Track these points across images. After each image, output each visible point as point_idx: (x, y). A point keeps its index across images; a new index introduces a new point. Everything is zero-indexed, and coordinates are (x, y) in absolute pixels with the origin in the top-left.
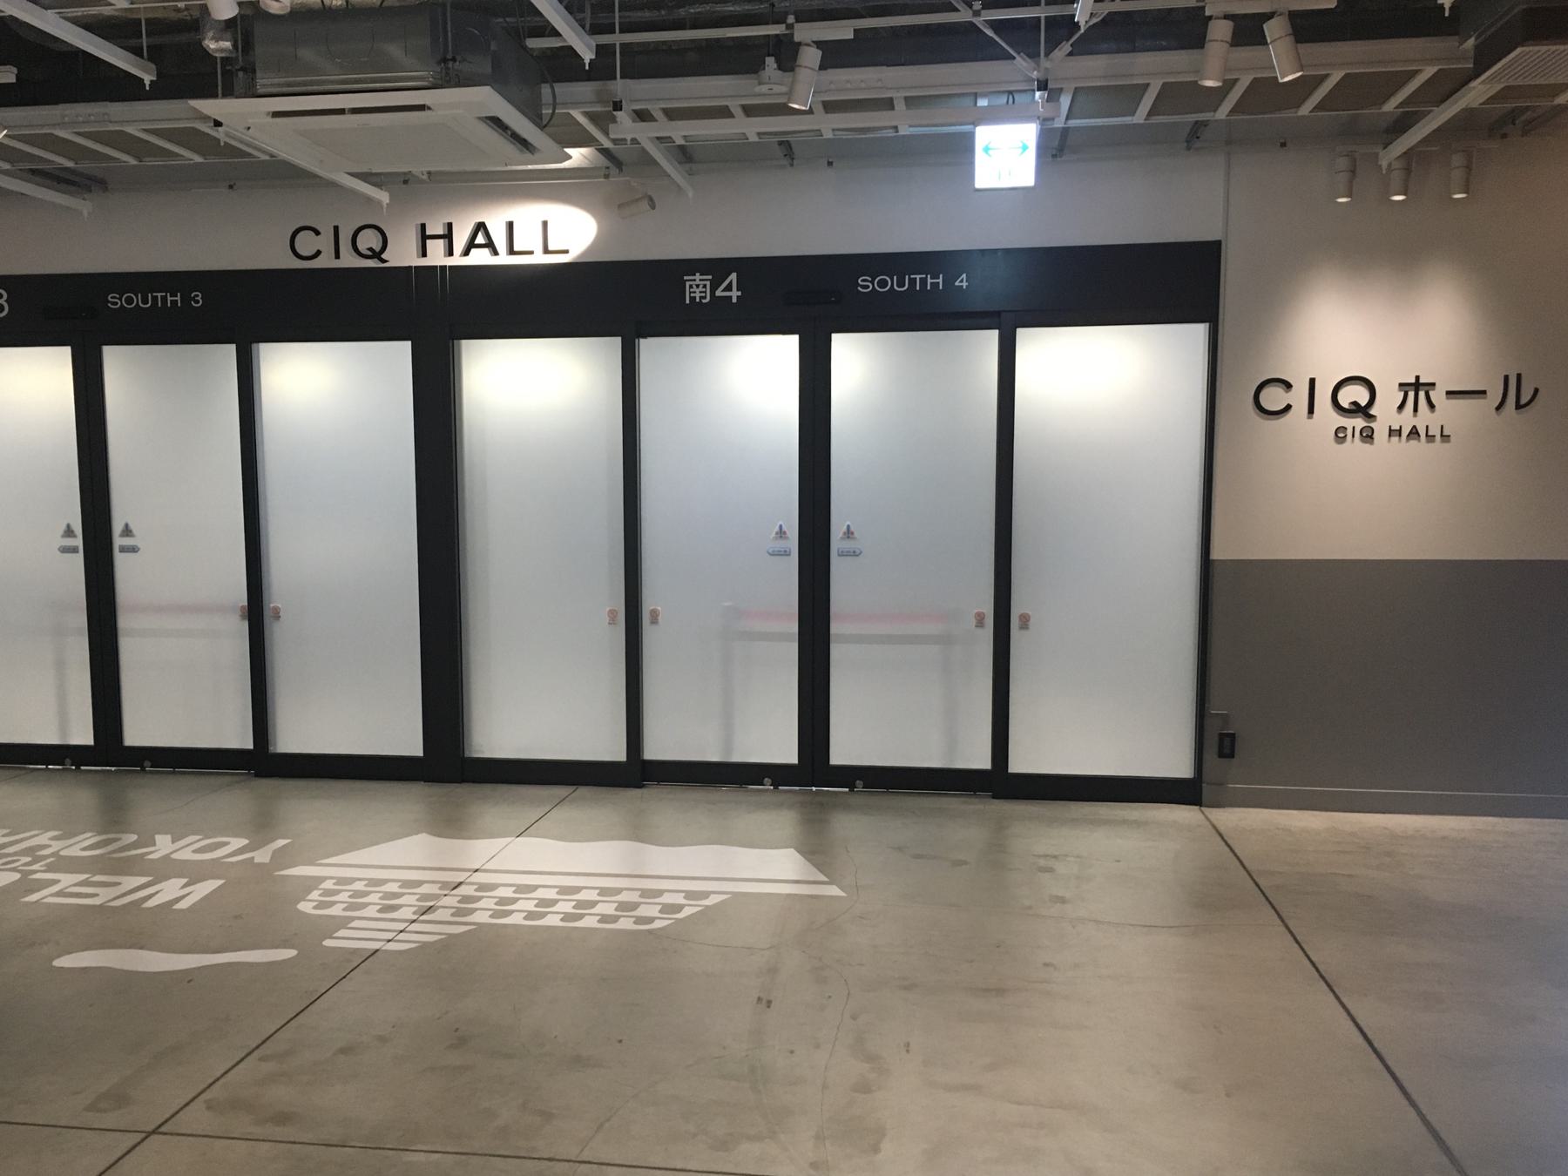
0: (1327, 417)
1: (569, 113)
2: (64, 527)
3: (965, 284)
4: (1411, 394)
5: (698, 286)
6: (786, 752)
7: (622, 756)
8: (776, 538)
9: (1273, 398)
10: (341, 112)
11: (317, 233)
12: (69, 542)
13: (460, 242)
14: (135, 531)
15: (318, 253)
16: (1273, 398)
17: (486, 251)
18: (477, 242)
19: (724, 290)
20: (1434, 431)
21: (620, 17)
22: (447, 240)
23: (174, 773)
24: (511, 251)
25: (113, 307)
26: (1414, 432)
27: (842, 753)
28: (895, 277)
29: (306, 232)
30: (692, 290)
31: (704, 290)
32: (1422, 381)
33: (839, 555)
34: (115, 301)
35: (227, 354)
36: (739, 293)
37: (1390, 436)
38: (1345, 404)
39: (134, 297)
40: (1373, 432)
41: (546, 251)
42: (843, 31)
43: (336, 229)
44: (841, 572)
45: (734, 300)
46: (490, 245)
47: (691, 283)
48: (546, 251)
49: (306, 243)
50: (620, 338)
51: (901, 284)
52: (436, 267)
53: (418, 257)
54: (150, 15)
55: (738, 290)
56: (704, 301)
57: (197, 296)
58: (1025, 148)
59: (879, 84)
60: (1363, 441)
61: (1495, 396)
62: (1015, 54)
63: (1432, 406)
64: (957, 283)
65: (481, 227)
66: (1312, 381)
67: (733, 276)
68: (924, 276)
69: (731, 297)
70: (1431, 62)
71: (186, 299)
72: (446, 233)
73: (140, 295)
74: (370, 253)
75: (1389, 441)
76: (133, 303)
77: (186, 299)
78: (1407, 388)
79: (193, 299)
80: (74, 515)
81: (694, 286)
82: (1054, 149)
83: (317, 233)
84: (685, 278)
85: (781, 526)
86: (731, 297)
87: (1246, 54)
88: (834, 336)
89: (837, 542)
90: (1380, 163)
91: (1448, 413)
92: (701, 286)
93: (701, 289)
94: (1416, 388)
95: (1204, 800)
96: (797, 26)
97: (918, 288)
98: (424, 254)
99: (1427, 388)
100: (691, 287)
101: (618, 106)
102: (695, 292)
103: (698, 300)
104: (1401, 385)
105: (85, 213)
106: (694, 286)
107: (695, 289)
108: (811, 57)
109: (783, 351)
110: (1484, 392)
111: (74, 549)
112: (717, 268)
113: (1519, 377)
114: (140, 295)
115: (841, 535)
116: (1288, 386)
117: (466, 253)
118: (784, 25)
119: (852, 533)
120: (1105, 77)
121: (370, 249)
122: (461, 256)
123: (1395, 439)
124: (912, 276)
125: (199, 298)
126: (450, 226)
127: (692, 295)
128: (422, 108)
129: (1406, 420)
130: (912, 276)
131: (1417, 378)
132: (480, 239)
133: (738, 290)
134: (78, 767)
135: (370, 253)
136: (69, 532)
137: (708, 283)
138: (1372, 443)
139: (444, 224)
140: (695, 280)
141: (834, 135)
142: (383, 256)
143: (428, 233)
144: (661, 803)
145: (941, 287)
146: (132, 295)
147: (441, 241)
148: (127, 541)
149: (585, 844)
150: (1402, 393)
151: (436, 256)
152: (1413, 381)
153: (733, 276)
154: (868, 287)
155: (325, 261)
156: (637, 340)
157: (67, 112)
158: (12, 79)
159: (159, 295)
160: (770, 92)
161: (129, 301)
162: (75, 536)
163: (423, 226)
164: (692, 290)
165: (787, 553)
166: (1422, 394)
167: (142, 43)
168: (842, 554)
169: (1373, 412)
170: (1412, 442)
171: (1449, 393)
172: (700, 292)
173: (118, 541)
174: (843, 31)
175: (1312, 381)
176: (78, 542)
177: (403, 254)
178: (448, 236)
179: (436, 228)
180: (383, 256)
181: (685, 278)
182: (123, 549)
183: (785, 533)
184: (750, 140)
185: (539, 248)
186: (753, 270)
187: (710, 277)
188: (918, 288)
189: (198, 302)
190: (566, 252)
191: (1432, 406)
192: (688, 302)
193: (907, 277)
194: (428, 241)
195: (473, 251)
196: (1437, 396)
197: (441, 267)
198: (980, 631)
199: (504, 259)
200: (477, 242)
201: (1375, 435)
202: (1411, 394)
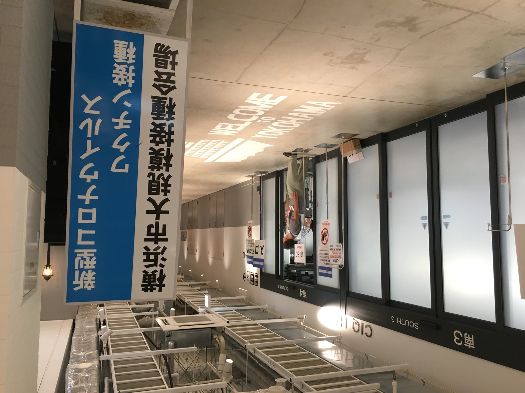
5: (469, 342)
7: (78, 271)
14: (422, 226)
39: (410, 326)
44: (425, 211)
47: (471, 344)
69: (84, 200)
73: (409, 326)
98: (366, 327)
100: (472, 343)
102: (468, 339)
114: (409, 326)
125: (457, 338)
131: (167, 212)
133: (91, 200)
136: (447, 225)
162: (444, 223)
173: (427, 221)
181: (474, 347)
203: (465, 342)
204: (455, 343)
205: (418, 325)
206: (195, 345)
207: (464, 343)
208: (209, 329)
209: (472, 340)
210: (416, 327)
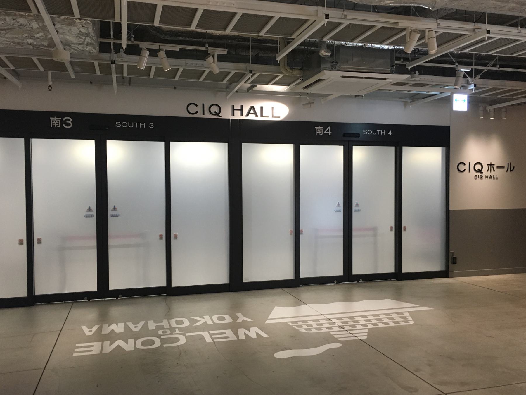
0: (473, 173)
1: (31, 58)
2: (88, 208)
3: (330, 133)
4: (490, 167)
5: (319, 130)
6: (93, 287)
7: (26, 295)
8: (337, 206)
9: (461, 167)
10: (362, 78)
11: (197, 105)
12: (90, 213)
13: (245, 112)
15: (197, 112)
16: (461, 167)
17: (254, 115)
18: (251, 112)
19: (327, 132)
20: (495, 177)
21: (252, 44)
22: (241, 111)
23: (368, 282)
24: (262, 116)
25: (117, 126)
26: (491, 177)
27: (114, 285)
28: (129, 123)
29: (212, 107)
30: (53, 122)
31: (58, 123)
32: (492, 164)
33: (111, 216)
34: (118, 124)
35: (21, 141)
36: (331, 133)
37: (486, 178)
38: (477, 169)
40: (482, 177)
41: (273, 117)
42: (175, 48)
43: (203, 105)
45: (330, 135)
46: (255, 113)
47: (317, 129)
48: (273, 117)
49: (192, 109)
50: (403, 147)
51: (131, 125)
52: (238, 119)
53: (231, 116)
54: (253, 37)
55: (331, 132)
56: (321, 135)
57: (152, 124)
58: (465, 101)
59: (432, 80)
60: (481, 179)
61: (506, 169)
62: (468, 77)
63: (494, 170)
64: (389, 133)
65: (252, 107)
66: (470, 163)
67: (329, 128)
68: (139, 123)
69: (329, 134)
70: (182, 66)
71: (147, 125)
72: (241, 109)
74: (215, 113)
75: (486, 179)
76: (126, 125)
77: (147, 125)
78: (489, 166)
79: (150, 125)
80: (93, 203)
81: (54, 121)
82: (473, 101)
83: (197, 105)
84: (316, 127)
85: (357, 203)
86: (329, 134)
87: (153, 59)
88: (107, 141)
89: (110, 212)
90: (487, 109)
91: (497, 172)
92: (57, 121)
93: (57, 122)
94: (491, 165)
95: (449, 276)
96: (209, 48)
97: (137, 127)
98: (233, 115)
99: (493, 166)
100: (317, 130)
101: (113, 62)
102: (318, 132)
103: (56, 126)
104: (488, 165)
105: (20, 87)
106: (54, 121)
107: (54, 122)
108: (162, 54)
109: (339, 151)
110: (504, 167)
111: (91, 216)
112: (325, 125)
113: (511, 163)
115: (355, 205)
116: (464, 164)
117: (247, 115)
118: (130, 41)
119: (116, 209)
120: (501, 86)
121: (215, 112)
122: (246, 116)
123: (487, 178)
124: (135, 123)
125: (152, 125)
126: (242, 106)
127: (318, 133)
128: (385, 79)
129: (489, 174)
130: (135, 123)
131: (491, 163)
132: (252, 111)
133: (331, 132)
134: (117, 298)
135: (215, 113)
137: (322, 129)
138: (482, 179)
139: (231, 105)
140: (318, 128)
141: (15, 68)
142: (220, 115)
143: (235, 108)
144: (306, 292)
145: (145, 127)
146: (126, 123)
147: (239, 111)
148: (114, 212)
149: (325, 305)
150: (488, 167)
151: (237, 116)
152: (490, 164)
153: (329, 128)
154: (119, 125)
155: (199, 115)
156: (30, 139)
157: (188, 62)
158: (226, 53)
159: (379, 131)
160: (122, 60)
161: (125, 125)
162: (92, 211)
163: (233, 106)
164: (53, 122)
165: (92, 216)
166: (492, 167)
167: (250, 44)
168: (355, 211)
169: (482, 171)
170: (490, 179)
171: (497, 167)
172: (57, 123)
174: (175, 48)
175: (470, 163)
176: (94, 213)
177: (226, 114)
178: (242, 110)
179: (237, 107)
180: (220, 115)
182: (112, 216)
183: (358, 205)
184: (41, 71)
185: (271, 116)
186: (335, 126)
187: (323, 128)
188: (137, 127)
189: (152, 126)
190: (279, 117)
191: (494, 170)
192: (316, 134)
193: (133, 123)
194: (235, 111)
195: (250, 115)
196: (495, 167)
197: (240, 119)
198: (392, 232)
199: (259, 118)
200: (251, 112)
201: (483, 178)
202: (490, 167)
203: (60, 120)
204: (69, 117)
205: (116, 126)
206: (409, 71)
207: (61, 120)
208: (342, 69)
209: (53, 123)
210: (366, 131)
